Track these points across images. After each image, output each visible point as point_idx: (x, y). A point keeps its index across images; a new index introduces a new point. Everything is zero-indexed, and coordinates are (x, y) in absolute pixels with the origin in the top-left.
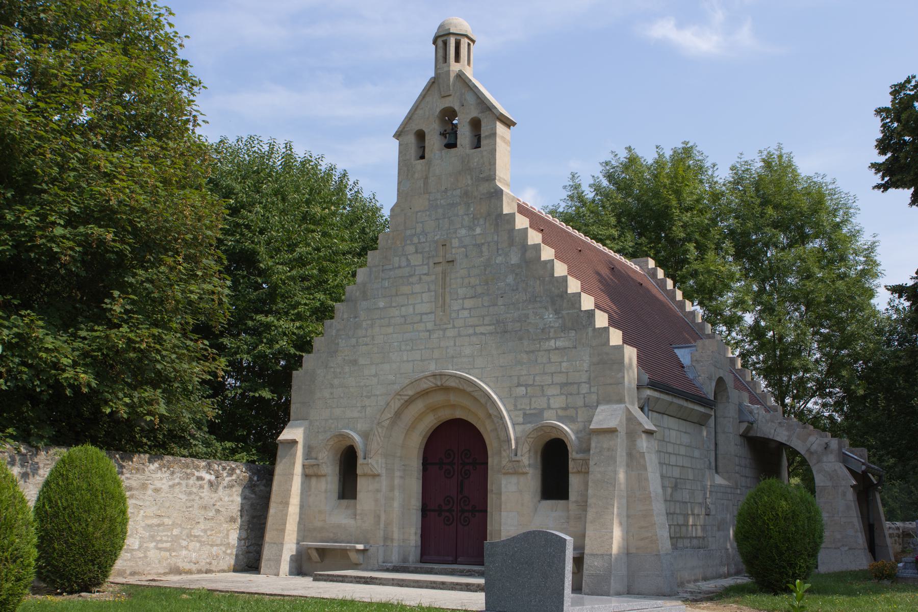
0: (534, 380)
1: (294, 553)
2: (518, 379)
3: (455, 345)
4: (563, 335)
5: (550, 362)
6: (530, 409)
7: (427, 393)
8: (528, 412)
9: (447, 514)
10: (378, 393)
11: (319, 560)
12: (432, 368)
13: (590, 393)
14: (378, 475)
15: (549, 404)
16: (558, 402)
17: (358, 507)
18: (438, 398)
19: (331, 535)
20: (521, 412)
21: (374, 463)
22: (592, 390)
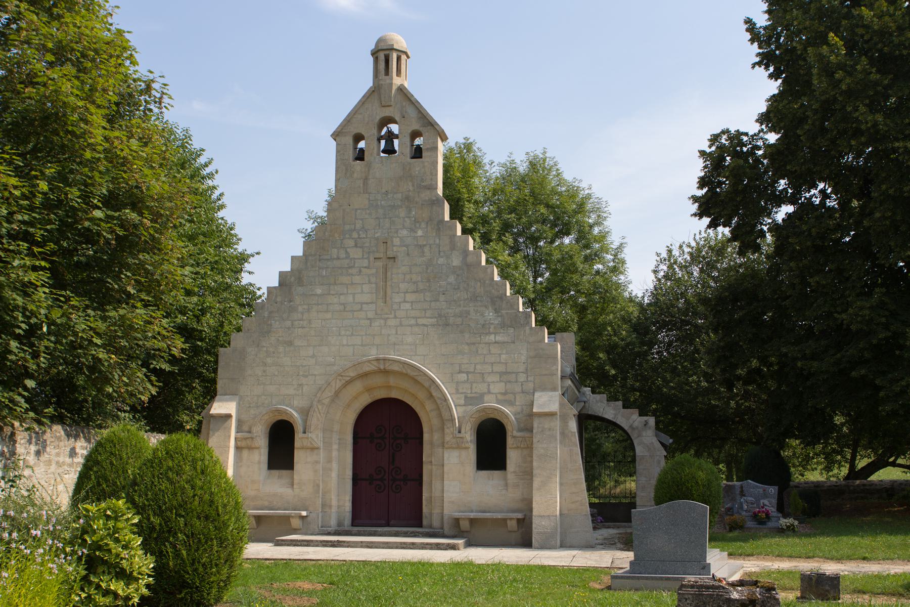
0: (475, 369)
8: (469, 395)
10: (316, 373)
12: (373, 353)
14: (318, 448)
15: (489, 389)
16: (497, 388)
17: (295, 477)
18: (378, 380)
19: (266, 504)
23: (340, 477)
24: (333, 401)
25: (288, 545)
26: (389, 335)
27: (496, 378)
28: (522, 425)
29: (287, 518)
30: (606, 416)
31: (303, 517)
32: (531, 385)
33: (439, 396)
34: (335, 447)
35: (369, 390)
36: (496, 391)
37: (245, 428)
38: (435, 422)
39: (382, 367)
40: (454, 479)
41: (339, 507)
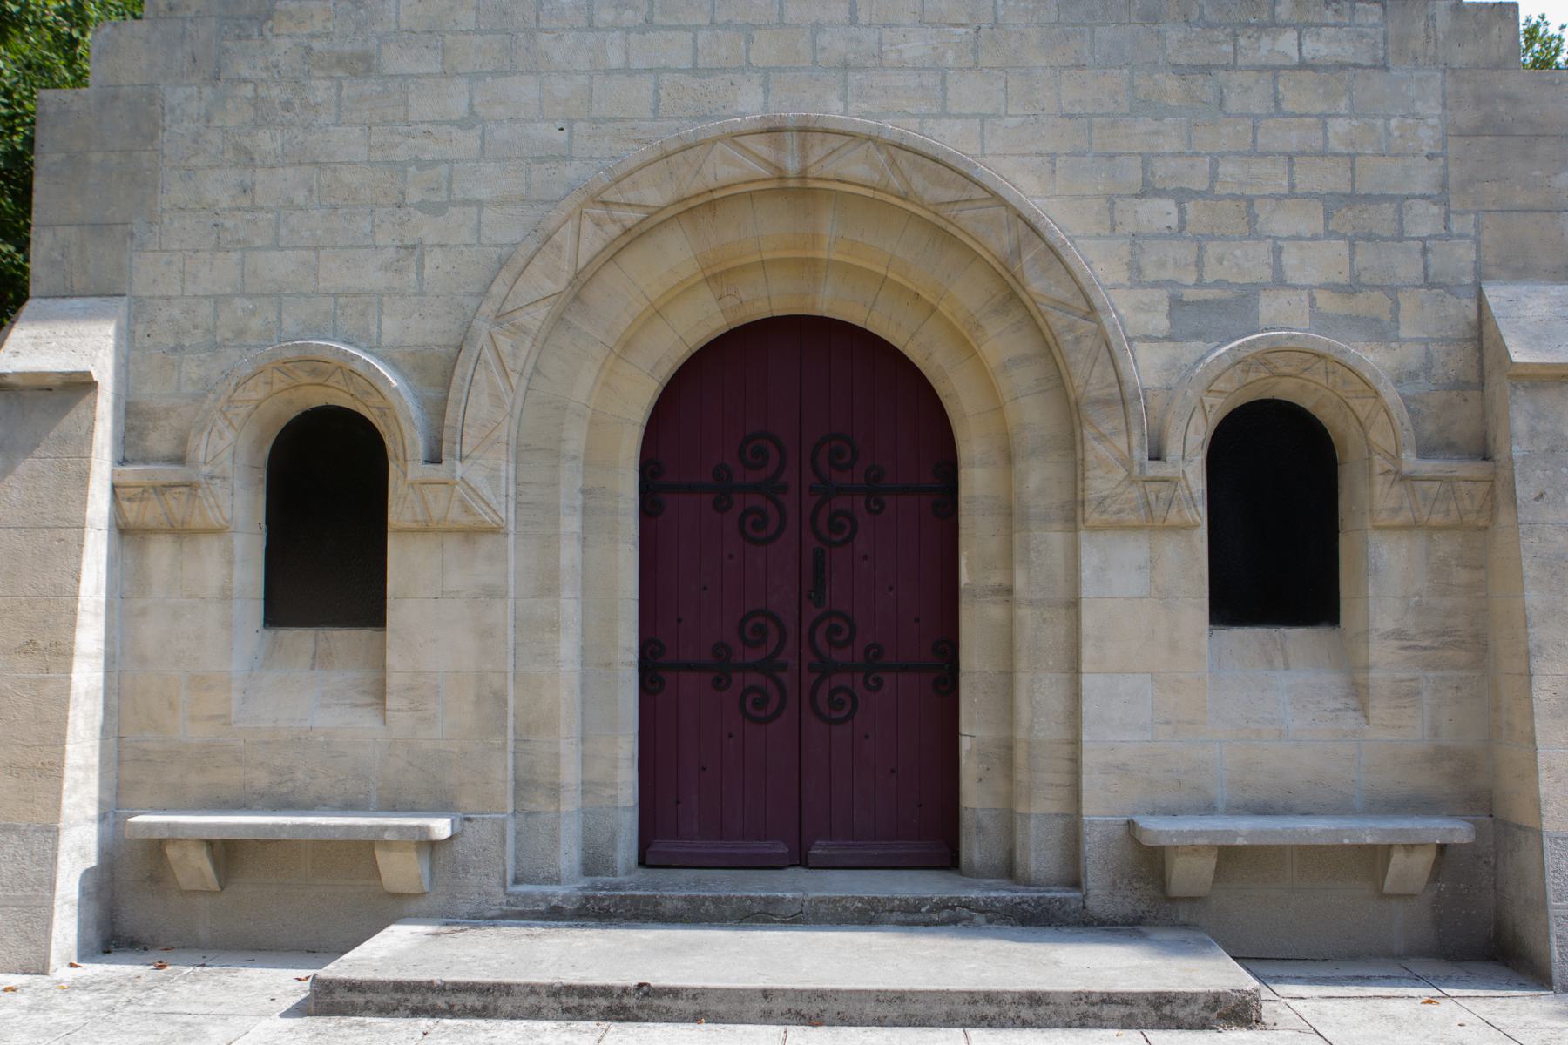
0: (1214, 177)
1: (93, 862)
2: (1145, 168)
3: (853, 21)
4: (1329, 16)
5: (1279, 111)
6: (1200, 283)
7: (712, 205)
8: (1189, 295)
9: (754, 679)
10: (483, 193)
11: (215, 886)
12: (750, 104)
13: (1447, 235)
14: (495, 531)
15: (1277, 268)
16: (1318, 263)
17: (392, 659)
18: (770, 230)
19: (262, 779)
20: (1162, 295)
21: (477, 477)
22: (1455, 227)
23: (593, 657)
24: (559, 320)
25: (384, 1011)
26: (817, 27)
27: (1309, 220)
28: (1429, 428)
29: (363, 849)
30: (388, 652)
31: (431, 847)
32: (1464, 254)
33: (1063, 293)
34: (571, 524)
35: (717, 277)
36: (1312, 276)
37: (160, 441)
38: (1032, 414)
39: (792, 165)
40: (1109, 665)
41: (587, 788)
